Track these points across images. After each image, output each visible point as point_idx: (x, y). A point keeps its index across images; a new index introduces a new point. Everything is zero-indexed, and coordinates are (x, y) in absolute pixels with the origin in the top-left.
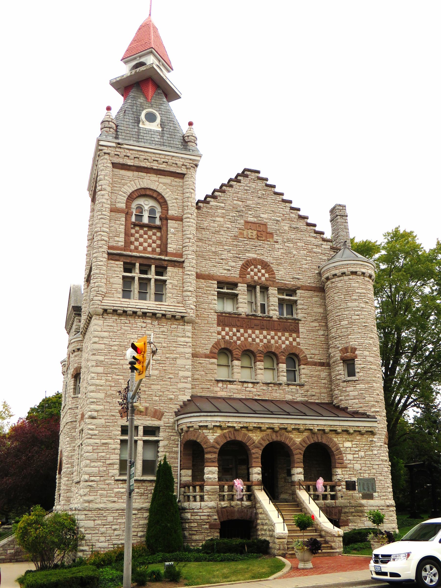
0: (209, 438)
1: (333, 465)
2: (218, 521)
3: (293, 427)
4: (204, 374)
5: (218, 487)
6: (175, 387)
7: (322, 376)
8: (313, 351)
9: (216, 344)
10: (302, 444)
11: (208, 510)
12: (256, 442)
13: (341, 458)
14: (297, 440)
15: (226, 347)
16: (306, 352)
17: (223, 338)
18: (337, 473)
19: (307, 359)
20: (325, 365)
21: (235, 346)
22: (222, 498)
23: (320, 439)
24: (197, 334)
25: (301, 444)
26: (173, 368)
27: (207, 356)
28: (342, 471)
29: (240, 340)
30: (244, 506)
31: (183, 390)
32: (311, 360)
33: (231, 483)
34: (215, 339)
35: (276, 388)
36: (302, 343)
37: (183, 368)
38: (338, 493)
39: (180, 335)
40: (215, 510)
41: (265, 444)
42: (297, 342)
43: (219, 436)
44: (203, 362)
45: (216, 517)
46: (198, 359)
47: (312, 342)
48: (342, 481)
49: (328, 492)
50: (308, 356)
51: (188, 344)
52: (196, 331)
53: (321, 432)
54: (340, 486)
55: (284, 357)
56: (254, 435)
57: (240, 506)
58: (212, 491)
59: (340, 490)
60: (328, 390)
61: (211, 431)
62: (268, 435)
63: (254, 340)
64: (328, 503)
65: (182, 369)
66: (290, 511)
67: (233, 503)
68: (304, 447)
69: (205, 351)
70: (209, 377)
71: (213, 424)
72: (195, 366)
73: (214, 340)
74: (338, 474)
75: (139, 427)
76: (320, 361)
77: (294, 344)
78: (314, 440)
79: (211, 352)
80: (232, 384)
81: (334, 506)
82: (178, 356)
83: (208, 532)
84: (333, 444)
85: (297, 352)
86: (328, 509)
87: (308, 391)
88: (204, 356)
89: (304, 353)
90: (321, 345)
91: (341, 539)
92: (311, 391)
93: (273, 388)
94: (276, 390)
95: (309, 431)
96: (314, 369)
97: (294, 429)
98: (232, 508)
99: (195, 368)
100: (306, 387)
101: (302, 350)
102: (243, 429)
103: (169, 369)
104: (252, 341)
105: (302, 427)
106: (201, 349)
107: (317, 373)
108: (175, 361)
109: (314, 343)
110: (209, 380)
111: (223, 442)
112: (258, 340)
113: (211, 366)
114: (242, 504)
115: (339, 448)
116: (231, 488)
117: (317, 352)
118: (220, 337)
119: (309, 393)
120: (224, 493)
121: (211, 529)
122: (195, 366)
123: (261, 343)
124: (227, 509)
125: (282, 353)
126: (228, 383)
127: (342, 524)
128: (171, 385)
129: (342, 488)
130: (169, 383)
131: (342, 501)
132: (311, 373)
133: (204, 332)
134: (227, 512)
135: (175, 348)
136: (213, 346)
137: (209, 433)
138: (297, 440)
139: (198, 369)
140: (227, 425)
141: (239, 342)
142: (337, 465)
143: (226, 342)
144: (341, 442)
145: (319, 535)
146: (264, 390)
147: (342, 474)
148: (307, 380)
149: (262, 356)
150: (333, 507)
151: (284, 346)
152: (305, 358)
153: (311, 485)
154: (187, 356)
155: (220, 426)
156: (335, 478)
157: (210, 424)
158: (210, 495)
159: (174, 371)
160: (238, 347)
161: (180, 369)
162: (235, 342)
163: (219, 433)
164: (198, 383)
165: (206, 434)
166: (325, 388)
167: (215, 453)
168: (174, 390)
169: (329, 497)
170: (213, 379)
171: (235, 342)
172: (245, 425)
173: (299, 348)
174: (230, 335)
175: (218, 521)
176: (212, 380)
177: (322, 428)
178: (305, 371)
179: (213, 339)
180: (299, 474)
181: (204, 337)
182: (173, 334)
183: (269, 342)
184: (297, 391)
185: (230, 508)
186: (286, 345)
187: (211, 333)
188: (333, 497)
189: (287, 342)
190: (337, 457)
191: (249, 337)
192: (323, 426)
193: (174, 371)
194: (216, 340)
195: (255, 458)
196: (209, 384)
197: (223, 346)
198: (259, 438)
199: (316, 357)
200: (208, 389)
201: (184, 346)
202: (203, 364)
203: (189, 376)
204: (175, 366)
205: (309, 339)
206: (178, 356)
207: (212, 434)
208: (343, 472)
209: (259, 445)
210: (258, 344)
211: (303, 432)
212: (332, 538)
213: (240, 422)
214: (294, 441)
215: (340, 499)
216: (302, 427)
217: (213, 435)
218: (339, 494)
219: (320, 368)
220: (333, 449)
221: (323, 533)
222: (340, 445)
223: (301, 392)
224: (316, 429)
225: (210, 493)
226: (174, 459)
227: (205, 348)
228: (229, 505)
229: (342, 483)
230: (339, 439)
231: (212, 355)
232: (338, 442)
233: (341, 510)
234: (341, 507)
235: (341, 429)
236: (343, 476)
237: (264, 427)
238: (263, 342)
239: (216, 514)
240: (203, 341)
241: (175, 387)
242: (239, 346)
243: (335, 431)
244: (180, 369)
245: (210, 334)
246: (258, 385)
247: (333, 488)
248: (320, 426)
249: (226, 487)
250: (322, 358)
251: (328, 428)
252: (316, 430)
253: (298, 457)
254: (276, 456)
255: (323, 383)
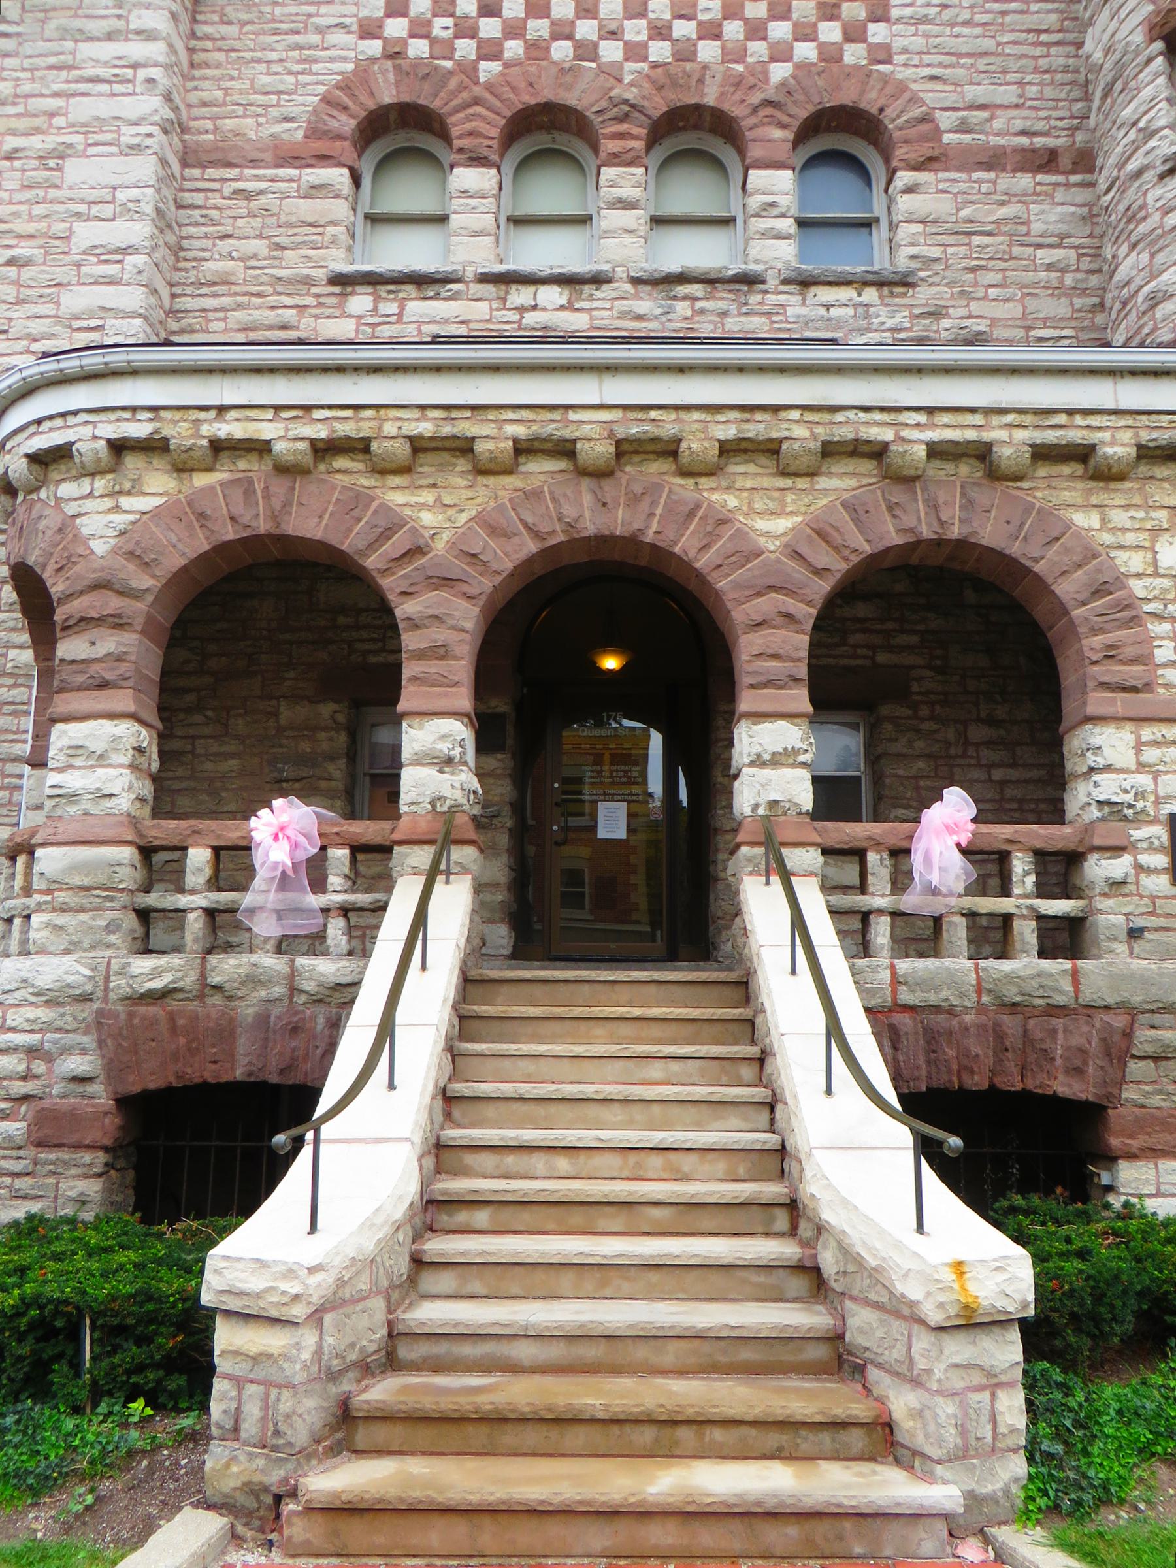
0: (85, 531)
1: (1069, 706)
2: (97, 1088)
3: (729, 432)
4: (265, 252)
5: (127, 853)
6: (49, 309)
7: (1036, 227)
8: (974, 92)
9: (345, 86)
10: (804, 550)
11: (31, 1013)
12: (440, 545)
13: (1129, 652)
14: (761, 524)
15: (406, 98)
16: (933, 96)
17: (394, 53)
18: (1092, 759)
19: (938, 132)
20: (1065, 161)
21: (462, 88)
22: (149, 927)
23: (955, 513)
24: (237, 45)
25: (797, 555)
26: (38, 210)
27: (291, 158)
28: (1139, 746)
29: (497, 56)
30: (310, 986)
31: (93, 323)
32: (967, 138)
33: (229, 831)
34: (344, 59)
35: (722, 305)
36: (906, 50)
37: (101, 204)
38: (1102, 904)
39: (93, 27)
40: (87, 1012)
41: (509, 555)
42: (872, 48)
43: (155, 514)
44: (263, 185)
45: (76, 1064)
46: (235, 172)
47: (969, 39)
48: (1141, 818)
49: (1022, 897)
50: (945, 120)
51: (142, 74)
52: (233, 30)
53: (964, 469)
54: (1117, 850)
55: (778, 134)
56: (428, 497)
57: (278, 991)
58: (77, 880)
59: (1116, 886)
60: (1078, 302)
61: (100, 484)
62: (533, 495)
63: (588, 51)
64: (1011, 978)
65: (95, 210)
66: (656, 1030)
67: (227, 968)
68: (819, 572)
69: (277, 128)
70: (294, 264)
71: (111, 429)
72: (214, 214)
73: (336, 66)
74: (1108, 768)
75: (1017, 924)
76: (1024, 141)
77: (848, 59)
78: (909, 521)
79: (314, 133)
80: (437, 297)
81: (1060, 1000)
82: (77, 139)
83: (17, 1166)
84: (1067, 550)
85: (870, 101)
86: (1011, 1024)
87: (936, 314)
88: (268, 156)
89: (914, 100)
90: (1038, 51)
91: (1008, 1351)
92: (963, 312)
93: (699, 305)
94: (724, 314)
95: (867, 466)
96: (984, 188)
97: (730, 450)
98: (217, 999)
99: (213, 222)
100: (923, 295)
101: (902, 87)
102: (341, 462)
103: (16, 215)
104: (577, 57)
105: (800, 432)
106: (250, 121)
107: (1004, 212)
108: (59, 168)
109: (988, 44)
110: (289, 281)
111: (183, 547)
112: (611, 51)
113: (306, 209)
114: (293, 973)
115: (1120, 580)
116: (233, 865)
117: (1008, 94)
118: (374, 47)
119: (945, 323)
120: (183, 901)
121: (40, 1144)
122: (214, 214)
123: (630, 66)
124: (173, 1004)
125: (769, 111)
126: (410, 290)
127: (1135, 1144)
128: (19, 302)
129: (1139, 868)
130: (12, 290)
131: (1136, 964)
132: (964, 213)
133: (276, 32)
134: (174, 1030)
135: (59, 102)
136: (327, 100)
137: (90, 495)
138: (761, 524)
139: (229, 229)
140: (206, 430)
141: (489, 69)
142: (1097, 701)
143: (425, 73)
144: (1130, 538)
145: (799, 1268)
146: (640, 318)
147: (1142, 767)
148: (936, 252)
149: (635, 131)
150: (1054, 1010)
151: (780, 72)
152: (924, 127)
153: (878, 845)
154: (129, 135)
155: (154, 447)
156: (1082, 798)
157: (87, 431)
158: (63, 910)
159: (43, 226)
160: (477, 91)
161: (82, 208)
162: (469, 70)
163: (156, 487)
164: (225, 301)
165: (71, 509)
166: (1058, 291)
167: (118, 623)
168: (35, 327)
169: (1026, 932)
170: (320, 274)
171: (469, 70)
172: (347, 429)
173: (885, 79)
174: (436, 31)
175: (97, 1088)
176: (307, 281)
177: (971, 435)
178: (919, 207)
179: (332, 60)
180: (776, 760)
181: (274, 56)
182: (52, 25)
183: (685, 53)
184: (867, 316)
185: (201, 997)
186: (798, 66)
187: (321, 31)
188: (1066, 938)
189: (806, 51)
190: (1098, 641)
191: (555, 37)
192: (978, 419)
193: (43, 226)
194: (350, 67)
195: (421, 655)
196: (288, 301)
197: (388, 96)
198: (463, 518)
199: (997, 124)
200: (284, 327)
201: (122, 76)
202: (263, 201)
203: (134, 240)
204: (53, 193)
205: (953, 25)
206: (77, 139)
207: (108, 503)
208: (1151, 755)
209: (459, 567)
210: (613, 73)
211: (812, 474)
212: (898, 1327)
213: (308, 408)
214: (740, 534)
215: (1122, 948)
216: (800, 435)
217: (117, 509)
218: (1110, 916)
219: (1024, 181)
220: (1066, 589)
221: (828, 1261)
222: (1121, 557)
223: (890, 323)
224: (914, 441)
225: (62, 896)
226: (14, 714)
227: (274, 112)
228: (189, 981)
229: (1136, 834)
230: (1119, 517)
231: (321, 147)
232: (1107, 538)
233: (1128, 1034)
234: (1133, 1013)
235: (1127, 436)
236: (1144, 780)
237: (493, 438)
238: (644, 59)
239: (88, 1041)
240: (265, 79)
241: (49, 309)
242: (489, 87)
243: (1082, 454)
244: (82, 208)
245: (315, 38)
246: (606, 291)
247: (1060, 870)
248: (946, 418)
249: (199, 857)
250: (1040, 126)
251: (1021, 435)
252: (921, 451)
253: (770, 647)
254: (606, 647)
255: (1050, 267)
